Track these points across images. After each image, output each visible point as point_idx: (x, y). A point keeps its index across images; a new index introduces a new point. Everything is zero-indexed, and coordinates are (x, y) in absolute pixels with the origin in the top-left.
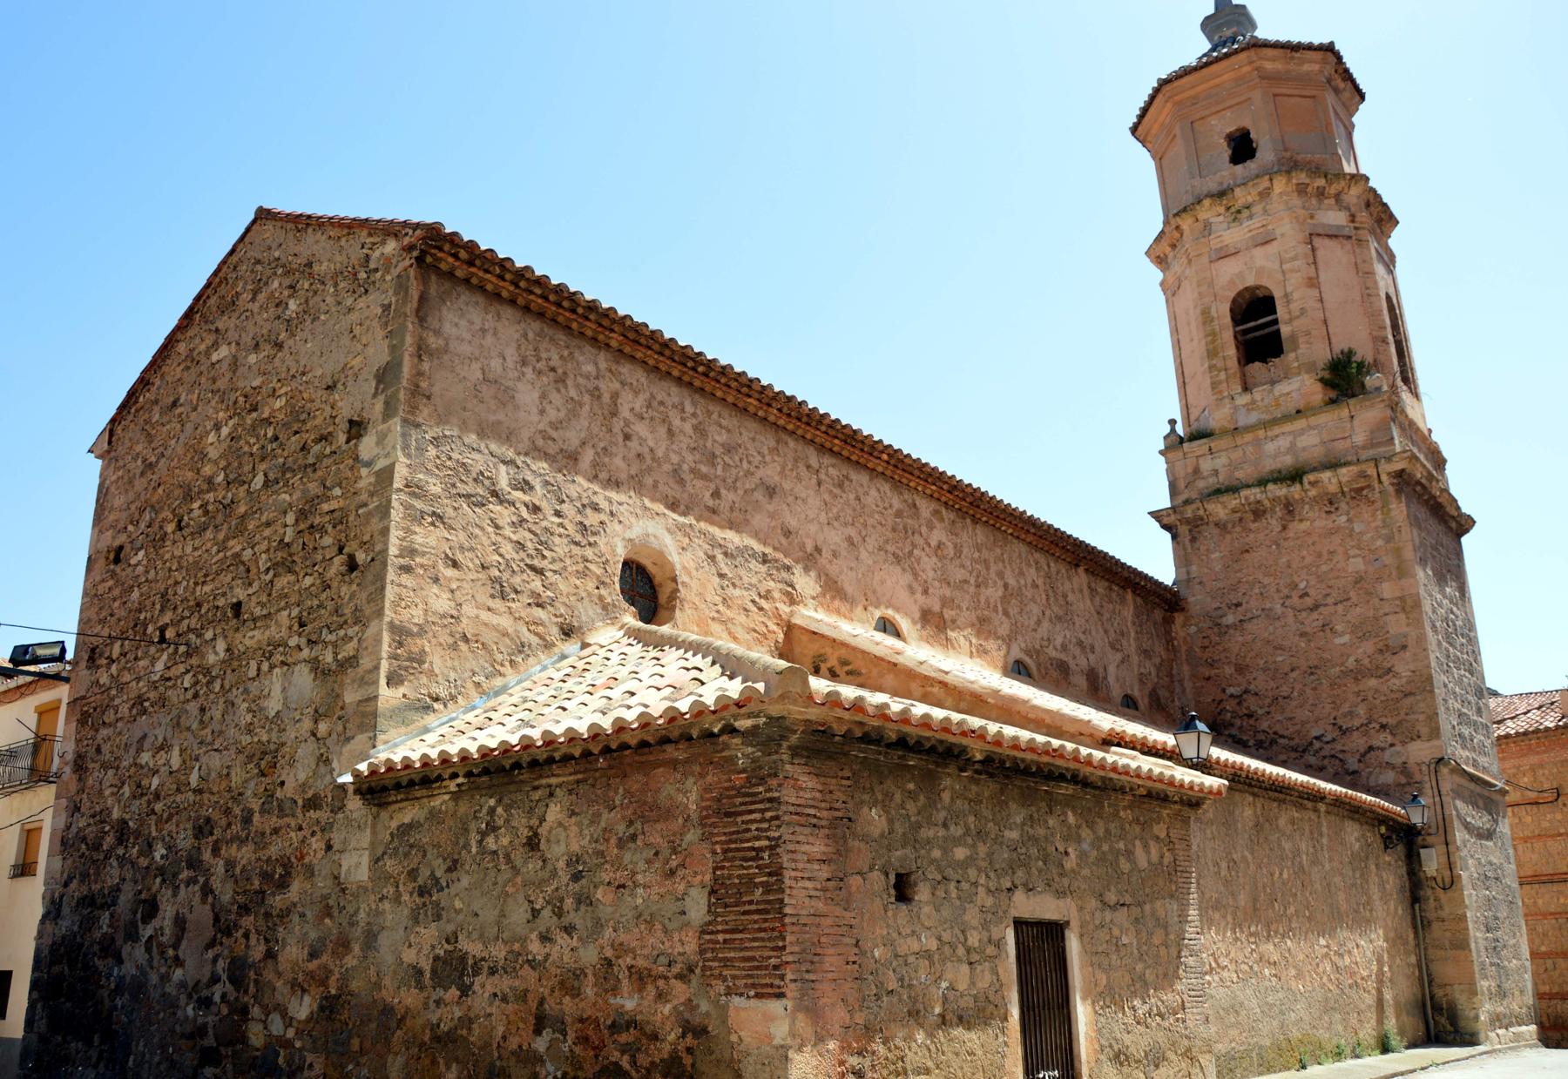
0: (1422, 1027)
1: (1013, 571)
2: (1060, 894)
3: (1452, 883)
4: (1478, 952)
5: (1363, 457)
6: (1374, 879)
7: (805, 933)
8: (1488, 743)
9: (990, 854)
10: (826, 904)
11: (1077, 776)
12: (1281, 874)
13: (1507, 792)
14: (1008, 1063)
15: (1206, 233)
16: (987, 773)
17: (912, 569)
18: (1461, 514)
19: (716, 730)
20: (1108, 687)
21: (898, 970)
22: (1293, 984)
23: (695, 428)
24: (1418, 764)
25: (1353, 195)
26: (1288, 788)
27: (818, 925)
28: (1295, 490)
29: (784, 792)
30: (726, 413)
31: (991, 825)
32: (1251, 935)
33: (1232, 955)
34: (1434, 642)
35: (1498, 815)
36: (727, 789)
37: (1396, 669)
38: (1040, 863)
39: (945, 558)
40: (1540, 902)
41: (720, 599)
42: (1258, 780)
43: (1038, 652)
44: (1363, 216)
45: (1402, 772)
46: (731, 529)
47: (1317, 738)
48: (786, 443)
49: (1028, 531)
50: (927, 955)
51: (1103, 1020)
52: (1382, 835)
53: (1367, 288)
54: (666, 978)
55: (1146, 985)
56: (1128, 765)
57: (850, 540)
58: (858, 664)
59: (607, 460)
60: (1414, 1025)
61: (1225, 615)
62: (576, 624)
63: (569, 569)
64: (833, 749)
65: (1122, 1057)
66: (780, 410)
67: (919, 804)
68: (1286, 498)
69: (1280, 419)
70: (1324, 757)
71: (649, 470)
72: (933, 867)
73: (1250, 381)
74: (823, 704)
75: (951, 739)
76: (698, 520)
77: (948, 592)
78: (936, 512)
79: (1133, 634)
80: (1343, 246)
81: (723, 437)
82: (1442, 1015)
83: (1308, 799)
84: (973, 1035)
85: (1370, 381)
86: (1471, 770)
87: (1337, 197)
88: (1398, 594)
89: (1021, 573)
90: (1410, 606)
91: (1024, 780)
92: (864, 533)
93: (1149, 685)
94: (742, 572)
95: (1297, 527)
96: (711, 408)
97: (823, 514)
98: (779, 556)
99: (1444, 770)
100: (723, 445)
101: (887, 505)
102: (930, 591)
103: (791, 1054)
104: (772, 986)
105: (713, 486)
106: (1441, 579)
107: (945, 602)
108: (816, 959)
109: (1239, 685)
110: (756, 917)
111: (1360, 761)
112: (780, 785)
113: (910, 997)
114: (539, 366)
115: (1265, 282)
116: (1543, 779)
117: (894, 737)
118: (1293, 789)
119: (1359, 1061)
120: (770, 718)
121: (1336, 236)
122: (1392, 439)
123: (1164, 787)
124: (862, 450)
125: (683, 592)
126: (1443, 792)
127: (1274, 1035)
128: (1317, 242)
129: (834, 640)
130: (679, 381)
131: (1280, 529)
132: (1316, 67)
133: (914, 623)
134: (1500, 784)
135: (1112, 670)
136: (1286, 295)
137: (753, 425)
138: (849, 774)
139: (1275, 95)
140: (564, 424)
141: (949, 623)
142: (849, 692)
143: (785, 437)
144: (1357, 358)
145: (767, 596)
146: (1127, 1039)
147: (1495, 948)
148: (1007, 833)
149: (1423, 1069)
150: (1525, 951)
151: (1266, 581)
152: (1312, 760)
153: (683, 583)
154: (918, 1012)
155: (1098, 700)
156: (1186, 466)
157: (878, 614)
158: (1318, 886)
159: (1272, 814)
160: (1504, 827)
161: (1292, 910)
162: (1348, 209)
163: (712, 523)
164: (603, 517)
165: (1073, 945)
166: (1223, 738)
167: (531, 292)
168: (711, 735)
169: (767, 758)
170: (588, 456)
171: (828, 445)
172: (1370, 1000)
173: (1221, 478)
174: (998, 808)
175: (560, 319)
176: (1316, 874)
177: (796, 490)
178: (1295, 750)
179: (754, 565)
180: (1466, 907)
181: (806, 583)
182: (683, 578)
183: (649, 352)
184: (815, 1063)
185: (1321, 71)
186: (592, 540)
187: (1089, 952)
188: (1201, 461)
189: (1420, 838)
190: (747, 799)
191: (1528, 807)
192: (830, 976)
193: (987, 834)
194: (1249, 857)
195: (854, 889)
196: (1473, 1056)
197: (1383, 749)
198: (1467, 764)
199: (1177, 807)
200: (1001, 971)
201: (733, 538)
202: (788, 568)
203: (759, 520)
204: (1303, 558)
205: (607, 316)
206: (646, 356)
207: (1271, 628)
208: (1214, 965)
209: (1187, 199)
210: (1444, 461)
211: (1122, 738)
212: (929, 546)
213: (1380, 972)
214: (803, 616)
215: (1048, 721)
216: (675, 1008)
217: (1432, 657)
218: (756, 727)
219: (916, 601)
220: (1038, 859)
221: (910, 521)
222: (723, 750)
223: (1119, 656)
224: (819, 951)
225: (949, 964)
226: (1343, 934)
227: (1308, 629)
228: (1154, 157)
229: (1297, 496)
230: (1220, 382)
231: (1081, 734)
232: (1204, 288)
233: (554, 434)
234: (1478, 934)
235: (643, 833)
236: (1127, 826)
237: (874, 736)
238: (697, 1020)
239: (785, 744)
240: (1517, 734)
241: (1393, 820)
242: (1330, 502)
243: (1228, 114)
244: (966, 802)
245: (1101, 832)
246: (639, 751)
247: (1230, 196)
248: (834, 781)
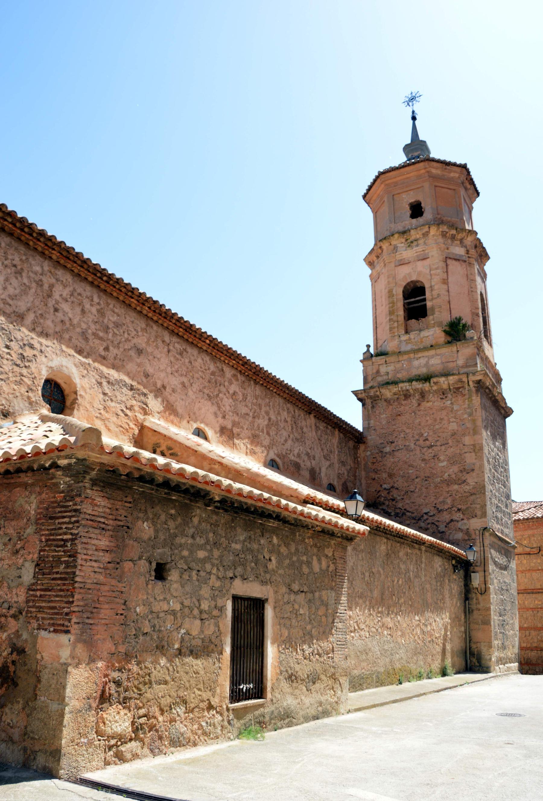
0: (464, 663)
1: (274, 412)
2: (264, 583)
3: (485, 591)
4: (495, 626)
5: (462, 372)
6: (447, 587)
7: (90, 594)
8: (509, 522)
9: (221, 557)
10: (105, 577)
11: (280, 516)
12: (398, 581)
13: (516, 547)
14: (220, 679)
15: (395, 251)
16: (223, 509)
17: (218, 404)
18: (507, 407)
19: (47, 465)
20: (320, 478)
21: (152, 621)
22: (399, 640)
23: (98, 311)
24: (474, 530)
25: (469, 240)
26: (406, 537)
27: (99, 590)
28: (426, 386)
29: (83, 506)
30: (118, 305)
31: (223, 539)
32: (379, 612)
33: (367, 623)
34: (488, 469)
35: (511, 558)
36: (52, 502)
37: (468, 481)
38: (253, 564)
39: (237, 400)
40: (526, 603)
41: (102, 407)
42: (390, 531)
43: (284, 456)
44: (473, 252)
45: (466, 534)
46: (113, 369)
47: (426, 513)
48: (152, 327)
49: (285, 392)
50: (174, 613)
51: (283, 656)
52: (453, 565)
53: (472, 288)
54: (6, 616)
55: (312, 637)
56: (311, 513)
57: (183, 384)
58: (176, 450)
59: (42, 321)
60: (460, 662)
61: (385, 447)
62: (11, 411)
63: (11, 379)
64: (120, 483)
65: (293, 678)
66: (149, 308)
67: (177, 523)
68: (422, 390)
69: (422, 349)
70: (428, 524)
71: (68, 330)
72: (182, 561)
73: (409, 328)
74: (110, 453)
75: (200, 486)
76: (94, 361)
77: (237, 419)
78: (234, 376)
79: (336, 452)
80: (461, 265)
81: (115, 318)
82: (474, 657)
83: (416, 543)
84: (199, 662)
85: (468, 334)
86: (500, 535)
87: (461, 241)
88: (472, 443)
89: (279, 414)
90: (477, 449)
91: (248, 516)
92: (192, 381)
93: (343, 480)
94: (118, 394)
95: (426, 405)
96: (109, 301)
97: (169, 368)
98: (141, 387)
99: (487, 534)
100: (114, 323)
101: (207, 368)
102: (227, 417)
103: (70, 669)
104: (63, 625)
105: (105, 344)
106: (494, 437)
107: (234, 424)
108: (95, 610)
109: (389, 484)
110: (59, 582)
111: (446, 527)
112: (82, 502)
113: (158, 638)
114: (6, 262)
115: (421, 279)
116: (533, 542)
117: (161, 480)
118: (408, 537)
119: (430, 680)
120: (78, 459)
121: (459, 260)
122: (477, 364)
123: (332, 528)
124: (195, 336)
125: (80, 400)
126: (485, 545)
127: (386, 666)
128: (449, 262)
129: (165, 436)
130: (92, 284)
131: (417, 405)
132: (457, 175)
133: (216, 432)
134: (513, 543)
135: (324, 470)
136: (431, 287)
137: (133, 314)
138: (131, 500)
139: (436, 186)
140: (18, 297)
141: (236, 435)
142: (161, 460)
143: (151, 323)
144: (463, 322)
145: (131, 408)
146: (297, 667)
147: (502, 625)
148: (233, 545)
149: (461, 685)
150: (517, 627)
151: (407, 431)
152: (422, 525)
153: (80, 395)
154: (163, 647)
155: (314, 485)
156: (373, 369)
157: (195, 426)
158: (417, 589)
159: (396, 550)
160: (513, 565)
161: (402, 600)
162: (466, 247)
163: (103, 364)
164: (35, 352)
165: (269, 613)
166: (379, 510)
167: (6, 220)
168: (45, 469)
169: (76, 485)
170: (30, 317)
171: (176, 331)
172: (439, 649)
173: (390, 376)
174: (229, 530)
175: (23, 238)
176: (416, 582)
177: (155, 353)
178: (414, 519)
179: (124, 390)
180: (491, 604)
181: (154, 404)
182: (81, 392)
183: (75, 265)
184: (86, 674)
185: (459, 177)
186: (27, 364)
187: (280, 619)
188: (381, 367)
189: (472, 568)
190: (63, 509)
191: (526, 555)
192: (103, 621)
193: (220, 544)
194: (382, 572)
195: (126, 570)
196: (487, 679)
197: (458, 521)
198: (498, 532)
199: (340, 540)
200: (221, 625)
201: (114, 374)
202: (145, 395)
203: (131, 366)
204: (427, 421)
205: (50, 240)
206: (73, 267)
207: (408, 456)
208: (356, 627)
209: (388, 233)
210: (501, 380)
211: (314, 500)
212: (229, 392)
213: (446, 635)
214: (151, 422)
215: (274, 488)
216: (9, 635)
217: (486, 476)
218: (70, 465)
219: (218, 422)
220: (252, 561)
221: (219, 378)
222: (52, 479)
223: (328, 463)
224: (97, 606)
225: (187, 619)
226: (428, 614)
227: (426, 458)
228: (373, 212)
229: (427, 389)
230: (394, 328)
231: (292, 496)
232: (391, 279)
233: (11, 302)
234: (495, 618)
235: (4, 527)
236: (309, 548)
237: (148, 478)
238: (19, 644)
239: (88, 477)
240: (524, 519)
241: (459, 557)
242: (443, 393)
243: (412, 193)
244: (209, 525)
245: (293, 550)
246: (6, 476)
247: (408, 234)
248: (120, 503)
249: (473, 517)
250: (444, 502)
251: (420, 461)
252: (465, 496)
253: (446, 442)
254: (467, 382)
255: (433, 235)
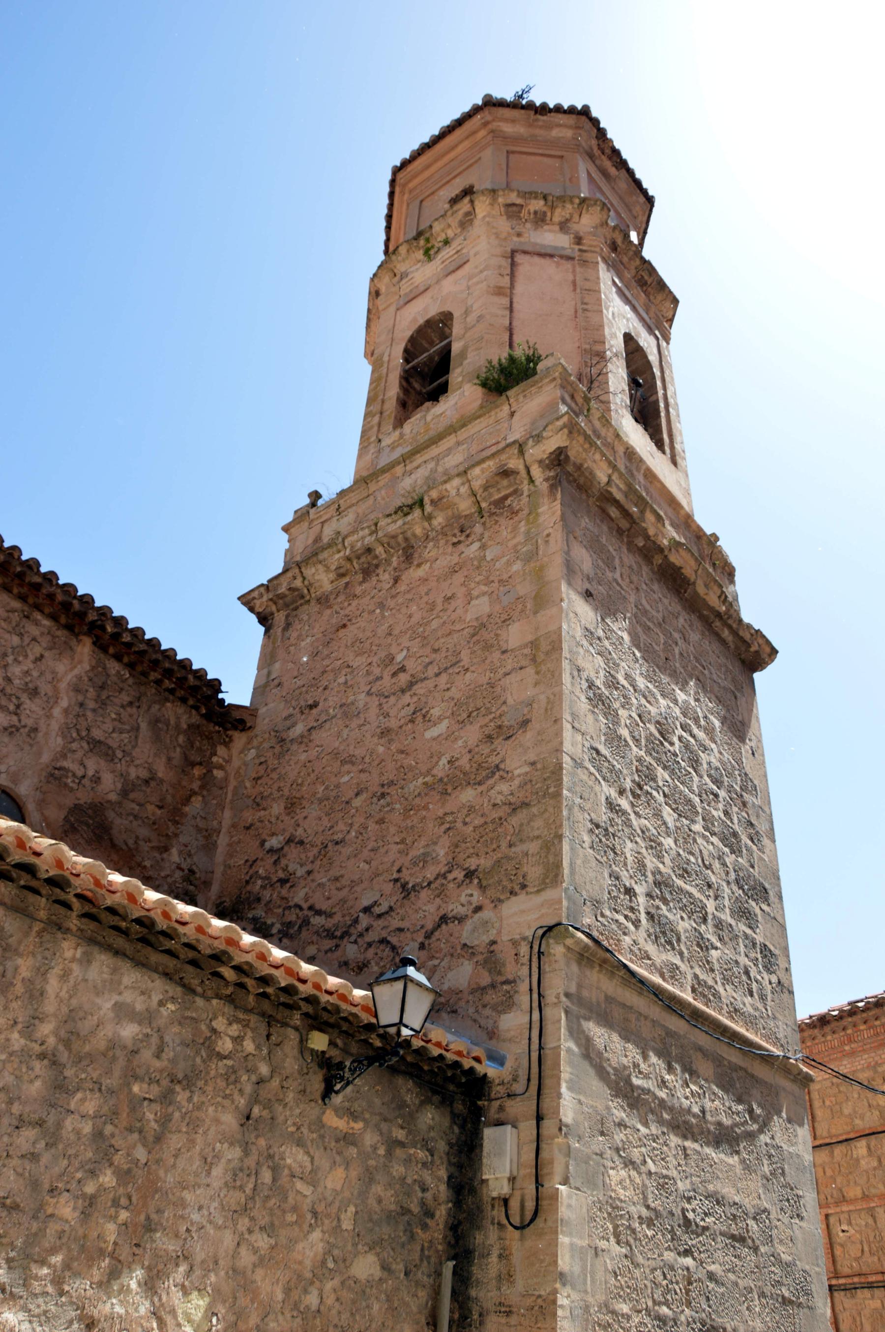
24: (515, 943)
70: (370, 945)
88: (530, 638)
111: (422, 946)
126: (550, 997)
152: (351, 951)
178: (330, 934)
197: (461, 919)
227: (393, 723)
249: (512, 893)
250: (424, 860)
251: (375, 740)
252: (493, 821)
253: (454, 660)
254: (523, 472)
255: (484, 217)
